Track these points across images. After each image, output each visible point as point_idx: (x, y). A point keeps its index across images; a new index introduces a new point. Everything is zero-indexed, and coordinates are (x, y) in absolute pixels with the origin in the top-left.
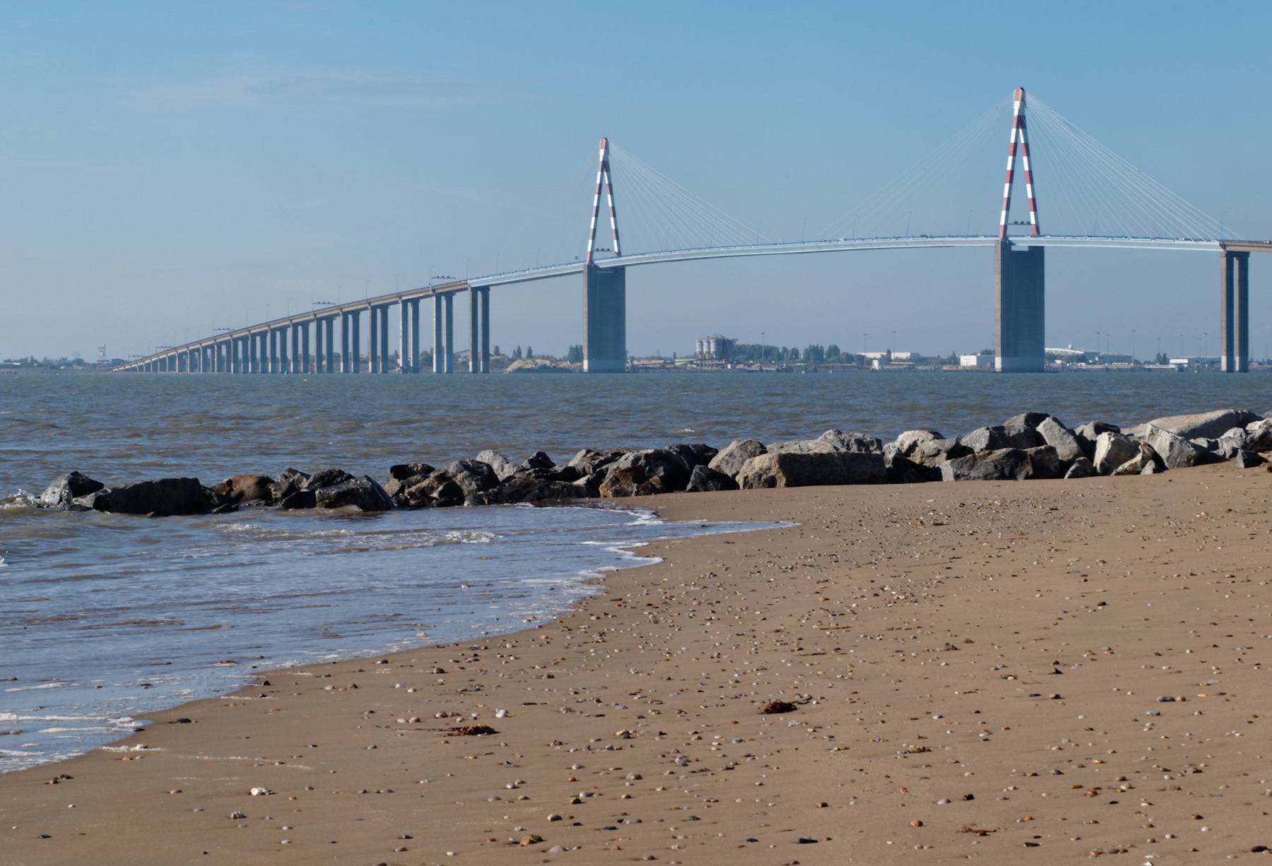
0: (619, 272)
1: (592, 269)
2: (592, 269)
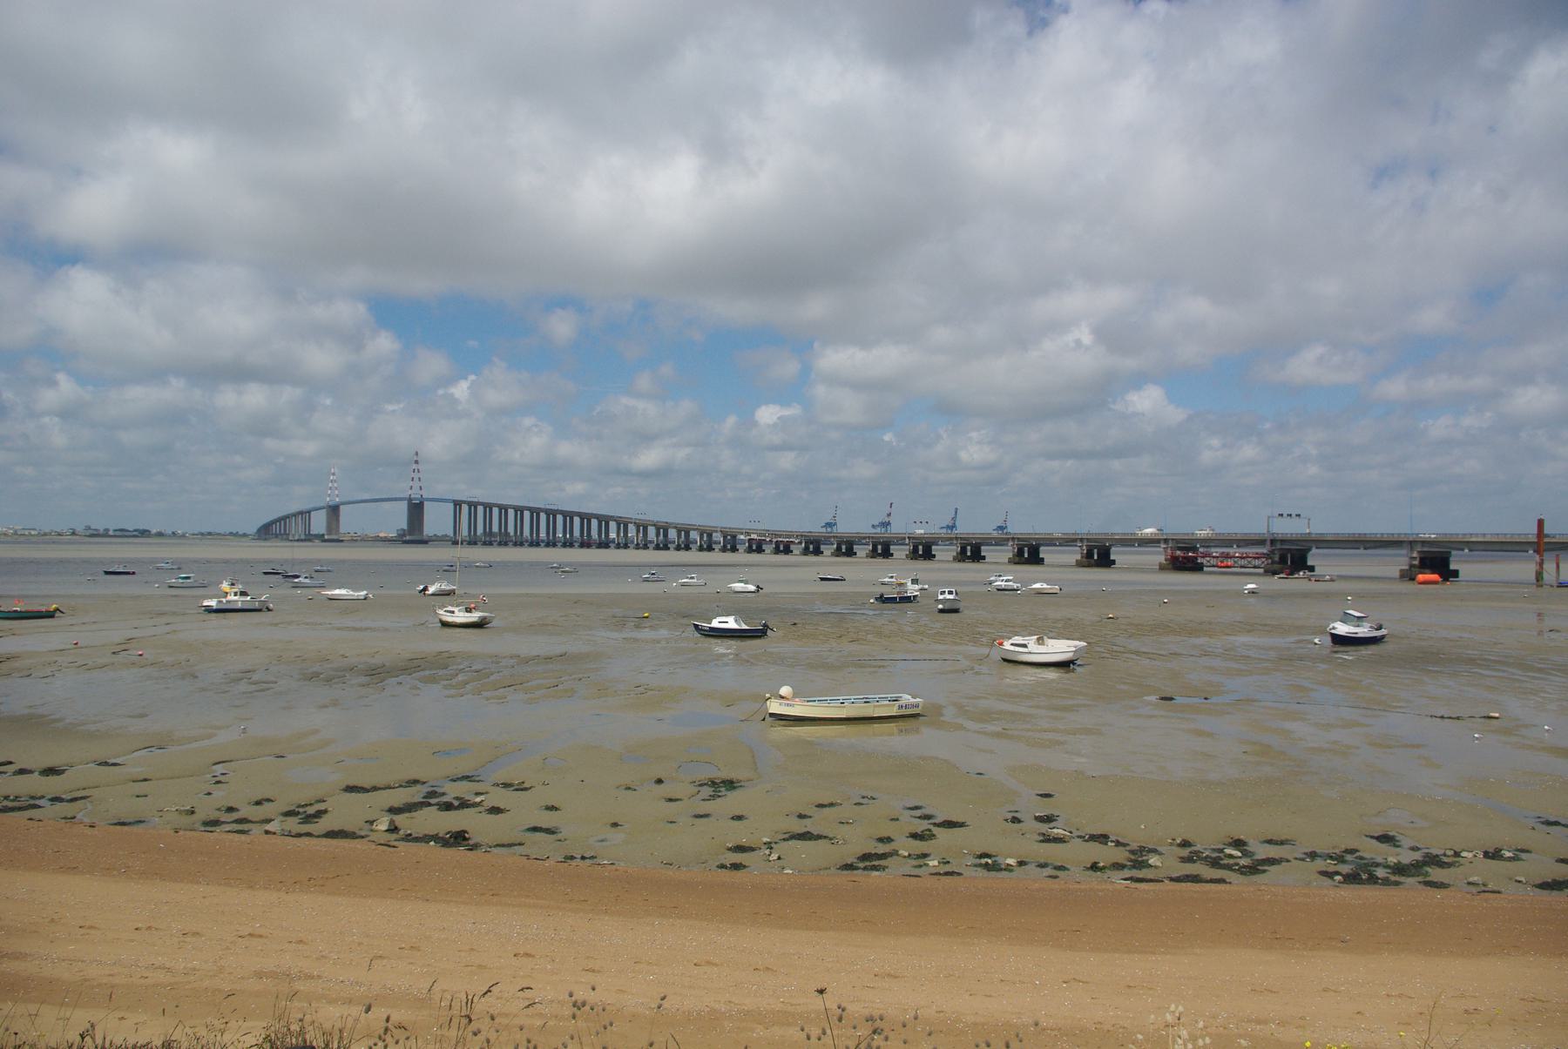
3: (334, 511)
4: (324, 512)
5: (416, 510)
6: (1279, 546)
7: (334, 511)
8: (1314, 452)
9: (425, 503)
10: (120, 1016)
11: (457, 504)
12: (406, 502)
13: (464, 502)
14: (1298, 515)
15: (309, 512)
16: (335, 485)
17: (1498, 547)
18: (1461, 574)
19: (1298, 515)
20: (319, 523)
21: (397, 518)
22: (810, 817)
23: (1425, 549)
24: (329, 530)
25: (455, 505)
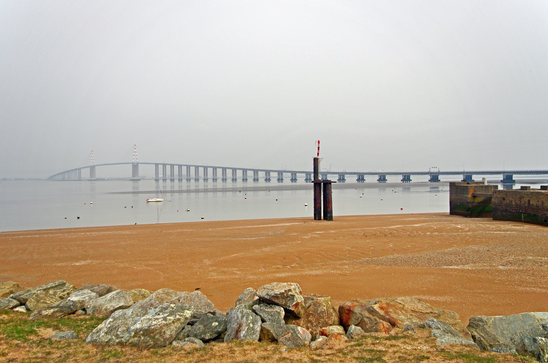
3: (92, 168)
4: (89, 168)
5: (135, 167)
6: (432, 174)
7: (92, 168)
8: (320, 178)
9: (139, 165)
10: (203, 219)
11: (157, 165)
12: (131, 164)
13: (161, 164)
14: (436, 167)
15: (80, 169)
16: (92, 158)
17: (144, 193)
18: (441, 181)
19: (436, 167)
20: (86, 174)
21: (128, 171)
22: (200, 289)
23: (467, 175)
24: (91, 176)
25: (156, 165)
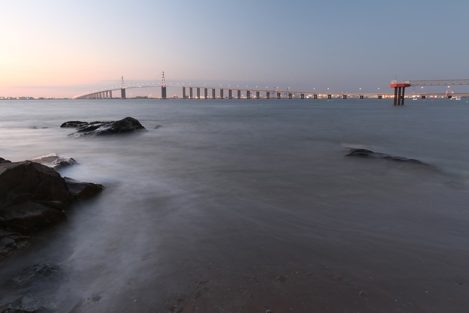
0: (165, 88)
1: (162, 87)
2: (162, 87)
20: (118, 94)
